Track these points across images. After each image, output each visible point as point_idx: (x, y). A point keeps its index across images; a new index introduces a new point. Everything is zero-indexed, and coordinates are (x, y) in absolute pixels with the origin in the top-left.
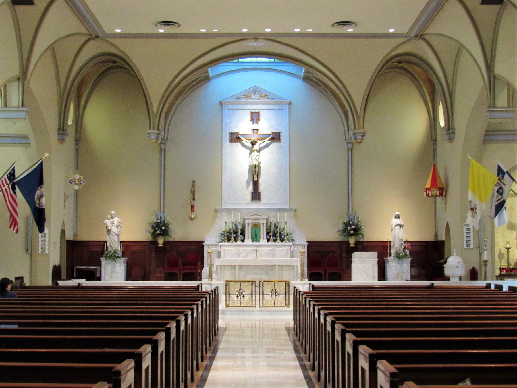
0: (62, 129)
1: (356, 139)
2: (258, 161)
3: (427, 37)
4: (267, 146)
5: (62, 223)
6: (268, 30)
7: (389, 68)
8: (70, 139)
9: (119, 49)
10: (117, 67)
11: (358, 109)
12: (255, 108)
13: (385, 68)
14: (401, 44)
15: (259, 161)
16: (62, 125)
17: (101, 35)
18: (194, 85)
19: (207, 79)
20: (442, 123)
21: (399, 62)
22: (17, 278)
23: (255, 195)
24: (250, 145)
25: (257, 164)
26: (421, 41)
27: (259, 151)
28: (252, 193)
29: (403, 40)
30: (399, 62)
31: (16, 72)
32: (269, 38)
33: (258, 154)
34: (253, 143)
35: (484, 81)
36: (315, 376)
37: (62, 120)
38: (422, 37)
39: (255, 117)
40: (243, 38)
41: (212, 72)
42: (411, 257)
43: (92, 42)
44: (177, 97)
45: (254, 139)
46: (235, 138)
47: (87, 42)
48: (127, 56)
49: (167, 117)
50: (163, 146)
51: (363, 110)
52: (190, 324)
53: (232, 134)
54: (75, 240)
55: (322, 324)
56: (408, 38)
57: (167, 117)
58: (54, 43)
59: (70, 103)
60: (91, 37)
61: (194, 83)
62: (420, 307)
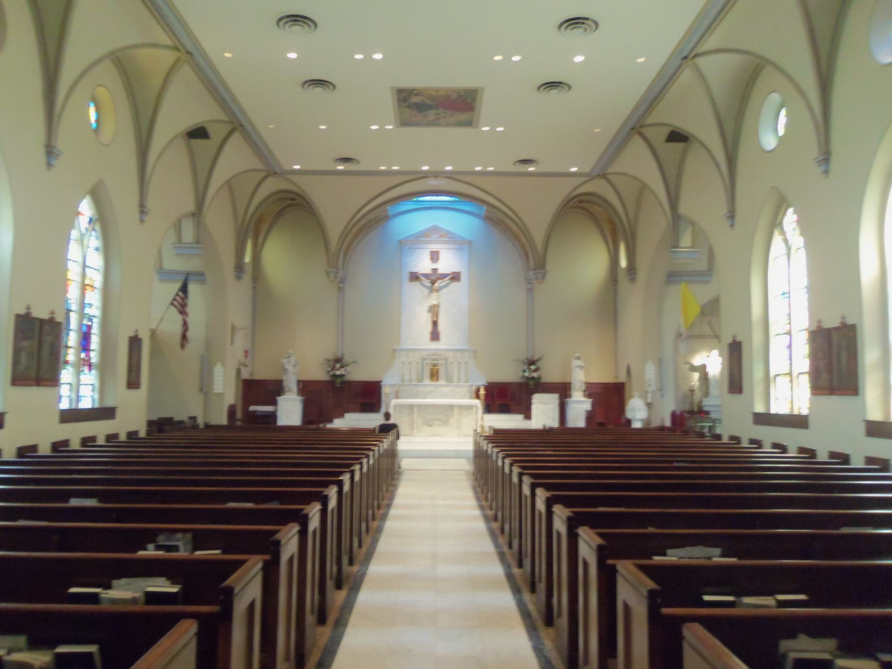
0: (239, 268)
3: (609, 177)
4: (446, 286)
6: (449, 168)
7: (571, 208)
8: (247, 277)
9: (295, 184)
10: (297, 205)
12: (434, 247)
14: (585, 182)
19: (387, 218)
20: (623, 263)
21: (580, 202)
24: (429, 285)
26: (603, 181)
29: (585, 179)
30: (580, 202)
31: (191, 207)
32: (449, 176)
34: (433, 283)
38: (605, 176)
39: (435, 256)
40: (425, 175)
41: (391, 210)
42: (647, 421)
44: (354, 238)
45: (433, 278)
49: (345, 256)
50: (341, 285)
52: (347, 492)
53: (412, 273)
54: (252, 378)
56: (590, 177)
57: (345, 256)
58: (231, 178)
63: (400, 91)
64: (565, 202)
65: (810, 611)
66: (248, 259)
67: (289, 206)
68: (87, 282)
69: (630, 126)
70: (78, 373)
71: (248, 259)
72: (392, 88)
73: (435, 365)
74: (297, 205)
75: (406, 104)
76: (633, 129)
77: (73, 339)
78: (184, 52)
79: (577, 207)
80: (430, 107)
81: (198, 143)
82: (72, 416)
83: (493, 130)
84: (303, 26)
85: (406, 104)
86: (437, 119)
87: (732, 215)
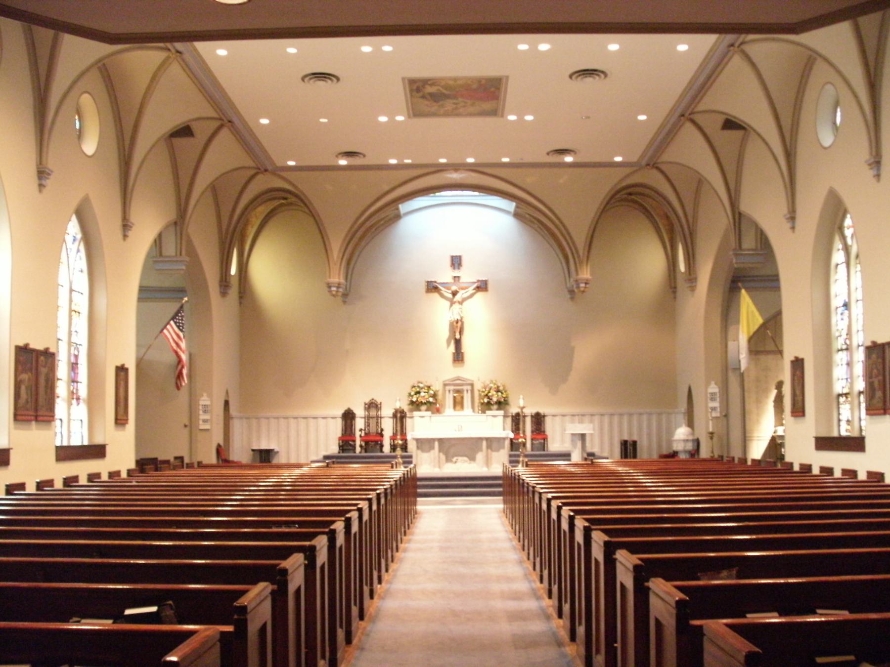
0: (224, 282)
1: (578, 287)
2: (460, 315)
4: (471, 296)
5: (225, 391)
7: (619, 201)
8: (234, 292)
9: (290, 183)
10: (291, 204)
11: (581, 253)
13: (612, 202)
14: (634, 172)
15: (462, 315)
16: (224, 277)
17: (270, 168)
18: (383, 224)
19: (398, 217)
20: (682, 267)
21: (630, 194)
22: (176, 458)
23: (457, 355)
24: (450, 296)
25: (459, 318)
26: (655, 171)
27: (461, 303)
28: (454, 353)
30: (630, 194)
32: (472, 168)
33: (460, 306)
34: (454, 294)
35: (729, 220)
36: (563, 627)
37: (224, 271)
38: (692, 116)
41: (404, 208)
43: (260, 176)
45: (454, 288)
46: (432, 287)
47: (253, 177)
48: (304, 194)
51: (586, 253)
52: (366, 521)
55: (554, 520)
59: (233, 249)
60: (259, 171)
61: (382, 222)
62: (765, 504)
63: (412, 82)
64: (613, 192)
65: (813, 618)
66: (233, 270)
67: (281, 205)
68: (74, 308)
69: (679, 111)
70: (70, 405)
71: (233, 270)
72: (403, 79)
73: (458, 391)
74: (291, 204)
75: (421, 94)
76: (683, 115)
77: (62, 371)
78: (173, 51)
79: (626, 200)
80: (447, 97)
81: (180, 142)
82: (66, 454)
83: (521, 119)
84: (325, 81)
85: (421, 94)
86: (456, 109)
87: (792, 218)
